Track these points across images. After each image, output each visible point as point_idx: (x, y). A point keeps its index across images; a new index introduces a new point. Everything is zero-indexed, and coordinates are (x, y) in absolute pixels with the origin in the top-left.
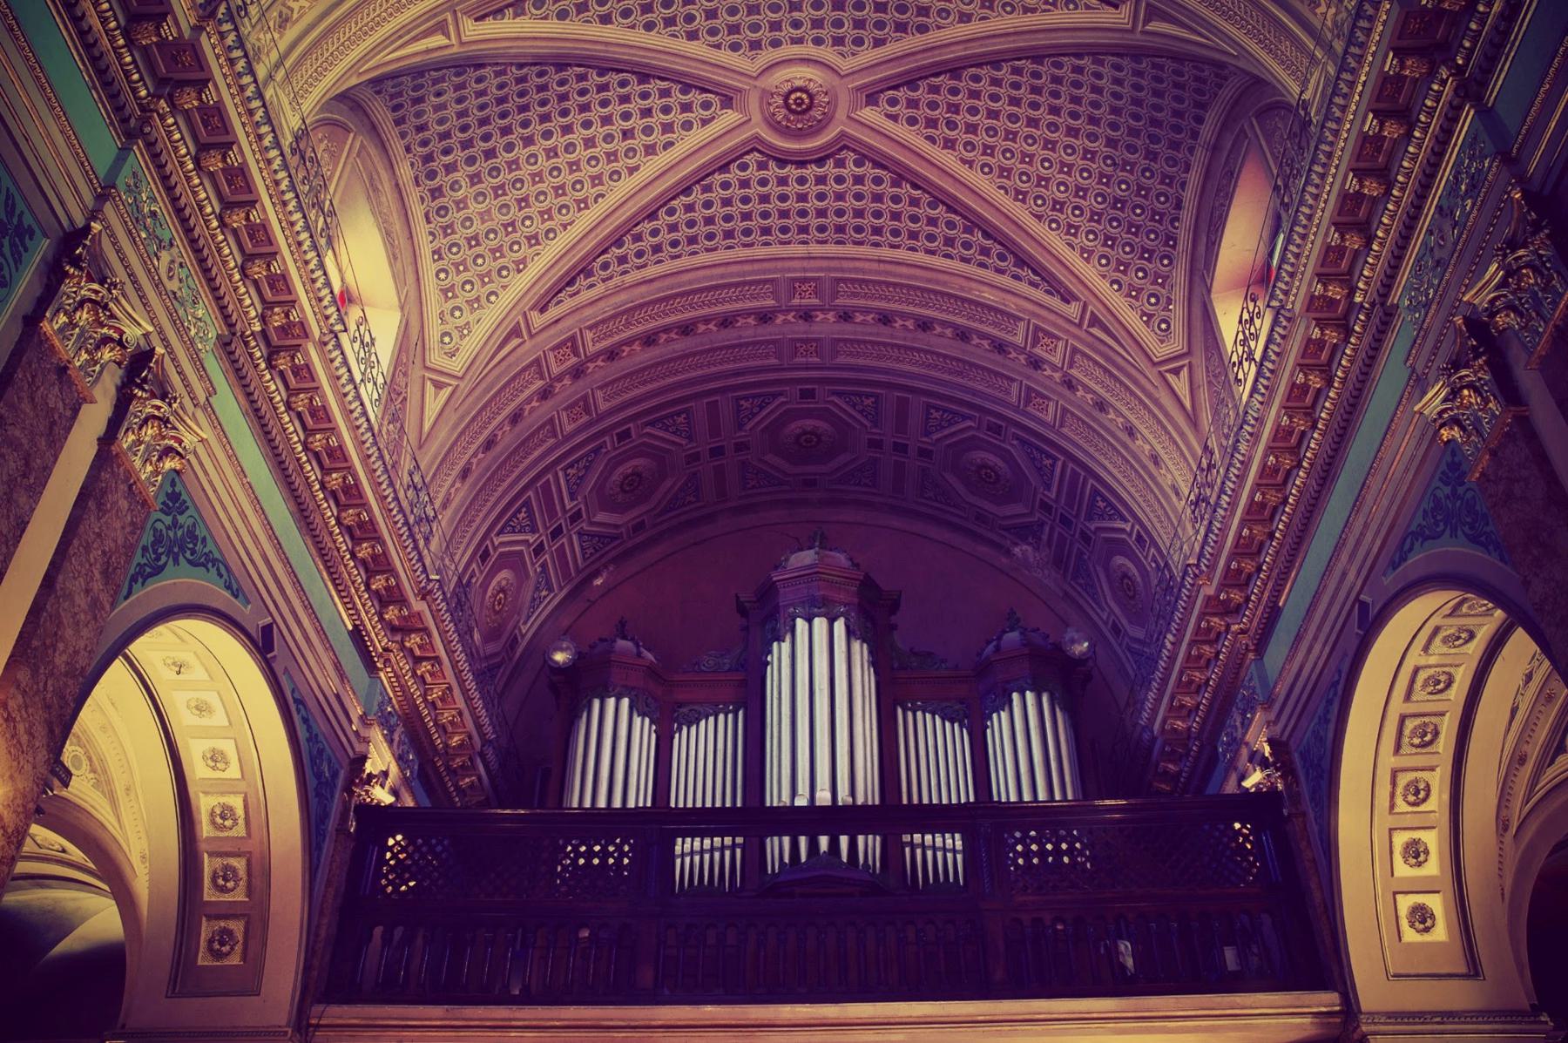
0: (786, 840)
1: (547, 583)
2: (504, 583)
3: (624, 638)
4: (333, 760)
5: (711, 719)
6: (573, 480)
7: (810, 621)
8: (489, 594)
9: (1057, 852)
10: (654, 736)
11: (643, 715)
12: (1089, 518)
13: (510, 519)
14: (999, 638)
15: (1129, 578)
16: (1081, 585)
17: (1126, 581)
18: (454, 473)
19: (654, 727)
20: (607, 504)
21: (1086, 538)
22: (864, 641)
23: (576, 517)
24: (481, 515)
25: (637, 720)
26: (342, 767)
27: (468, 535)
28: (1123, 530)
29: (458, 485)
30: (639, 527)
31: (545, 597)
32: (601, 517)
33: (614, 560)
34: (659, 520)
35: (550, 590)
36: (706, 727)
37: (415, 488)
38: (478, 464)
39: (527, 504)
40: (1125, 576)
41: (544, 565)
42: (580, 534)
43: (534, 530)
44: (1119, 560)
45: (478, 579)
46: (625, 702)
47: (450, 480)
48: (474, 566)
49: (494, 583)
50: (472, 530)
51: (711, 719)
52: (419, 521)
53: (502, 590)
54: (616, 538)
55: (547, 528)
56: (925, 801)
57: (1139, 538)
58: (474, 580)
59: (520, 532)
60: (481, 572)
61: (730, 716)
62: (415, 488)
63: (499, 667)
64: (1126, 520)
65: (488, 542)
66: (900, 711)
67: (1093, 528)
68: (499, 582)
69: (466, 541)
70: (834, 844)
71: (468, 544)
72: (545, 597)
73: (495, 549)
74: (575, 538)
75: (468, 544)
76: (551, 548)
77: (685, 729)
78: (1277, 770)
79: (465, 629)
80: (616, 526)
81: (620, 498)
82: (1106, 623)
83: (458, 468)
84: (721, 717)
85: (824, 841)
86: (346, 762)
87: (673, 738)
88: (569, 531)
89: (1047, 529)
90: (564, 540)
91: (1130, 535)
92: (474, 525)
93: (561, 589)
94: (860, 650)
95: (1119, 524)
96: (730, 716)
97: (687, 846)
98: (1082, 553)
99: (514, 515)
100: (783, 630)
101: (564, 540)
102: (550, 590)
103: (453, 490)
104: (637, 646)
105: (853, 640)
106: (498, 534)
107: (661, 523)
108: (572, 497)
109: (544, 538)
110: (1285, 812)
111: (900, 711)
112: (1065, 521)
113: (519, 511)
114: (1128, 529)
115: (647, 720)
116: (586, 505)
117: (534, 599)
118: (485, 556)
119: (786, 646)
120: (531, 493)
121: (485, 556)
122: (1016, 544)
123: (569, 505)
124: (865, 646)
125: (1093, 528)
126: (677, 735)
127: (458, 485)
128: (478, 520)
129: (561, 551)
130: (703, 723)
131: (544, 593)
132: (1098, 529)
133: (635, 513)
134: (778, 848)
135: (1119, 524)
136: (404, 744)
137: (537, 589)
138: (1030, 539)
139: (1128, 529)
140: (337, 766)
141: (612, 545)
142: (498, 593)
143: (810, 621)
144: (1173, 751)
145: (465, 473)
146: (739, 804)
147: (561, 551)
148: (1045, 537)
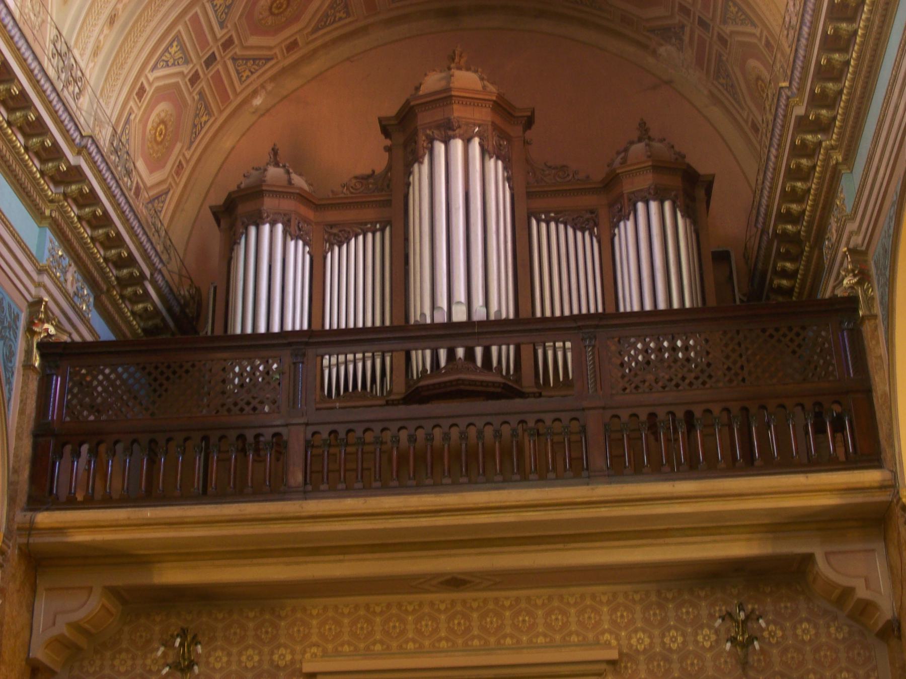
0: (428, 353)
1: (206, 108)
2: (163, 115)
3: (277, 165)
4: (13, 306)
5: (361, 238)
6: (222, 8)
7: (446, 142)
8: (149, 126)
9: (674, 349)
10: (308, 257)
11: (296, 238)
12: (724, 21)
13: (162, 54)
14: (626, 150)
15: (763, 81)
16: (722, 85)
17: (760, 83)
18: (101, 22)
19: (307, 249)
20: (258, 29)
21: (723, 41)
22: (498, 158)
23: (228, 44)
24: (133, 55)
25: (292, 244)
26: (22, 311)
27: (122, 78)
28: (753, 35)
29: (106, 31)
30: (292, 46)
31: (206, 122)
32: (254, 40)
33: (273, 79)
34: (311, 38)
35: (210, 113)
36: (356, 245)
37: (60, 55)
38: (124, 9)
39: (178, 37)
40: (758, 78)
41: (201, 94)
42: (234, 59)
43: (187, 61)
44: (753, 63)
45: (137, 115)
46: (280, 227)
47: (97, 30)
48: (131, 103)
49: (153, 117)
50: (124, 72)
51: (361, 238)
52: (67, 84)
53: (163, 122)
54: (272, 59)
55: (199, 57)
56: (548, 314)
57: (768, 44)
58: (132, 117)
59: (174, 65)
60: (139, 108)
61: (378, 235)
62: (60, 55)
63: (167, 193)
64: (755, 26)
65: (143, 79)
66: (534, 222)
67: (728, 32)
68: (159, 115)
69: (120, 82)
70: (470, 354)
71: (123, 84)
72: (206, 122)
73: (150, 84)
74: (230, 64)
75: (123, 84)
76: (206, 76)
77: (336, 249)
78: (855, 276)
79: (124, 172)
80: (270, 48)
81: (270, 20)
82: (746, 122)
83: (104, 16)
84: (370, 236)
85: (460, 352)
86: (24, 306)
87: (325, 258)
88: (222, 57)
89: (687, 30)
90: (219, 67)
91: (760, 40)
92: (127, 67)
93: (221, 112)
94: (495, 168)
95: (749, 29)
96: (378, 235)
97: (334, 360)
98: (720, 55)
99: (166, 50)
100: (421, 152)
101: (219, 67)
102: (210, 113)
103: (102, 38)
104: (288, 173)
105: (487, 157)
106: (152, 70)
107: (315, 39)
108: (222, 25)
109: (198, 67)
110: (861, 313)
111: (534, 222)
112: (702, 23)
113: (171, 45)
114: (758, 34)
115: (300, 243)
116: (237, 31)
117: (195, 126)
118: (141, 92)
119: (425, 167)
120: (180, 27)
121: (141, 92)
122: (661, 45)
123: (219, 33)
124: (500, 163)
125: (728, 32)
126: (329, 255)
127: (106, 31)
128: (130, 61)
129: (217, 77)
130: (353, 241)
131: (204, 118)
132: (732, 33)
133: (287, 33)
134: (422, 359)
135: (749, 29)
136: (78, 281)
137: (197, 115)
138: (674, 40)
139: (758, 34)
140: (16, 310)
141: (267, 66)
142: (158, 125)
143: (446, 142)
144: (788, 252)
145: (112, 20)
146: (388, 323)
147: (217, 77)
148: (686, 38)
